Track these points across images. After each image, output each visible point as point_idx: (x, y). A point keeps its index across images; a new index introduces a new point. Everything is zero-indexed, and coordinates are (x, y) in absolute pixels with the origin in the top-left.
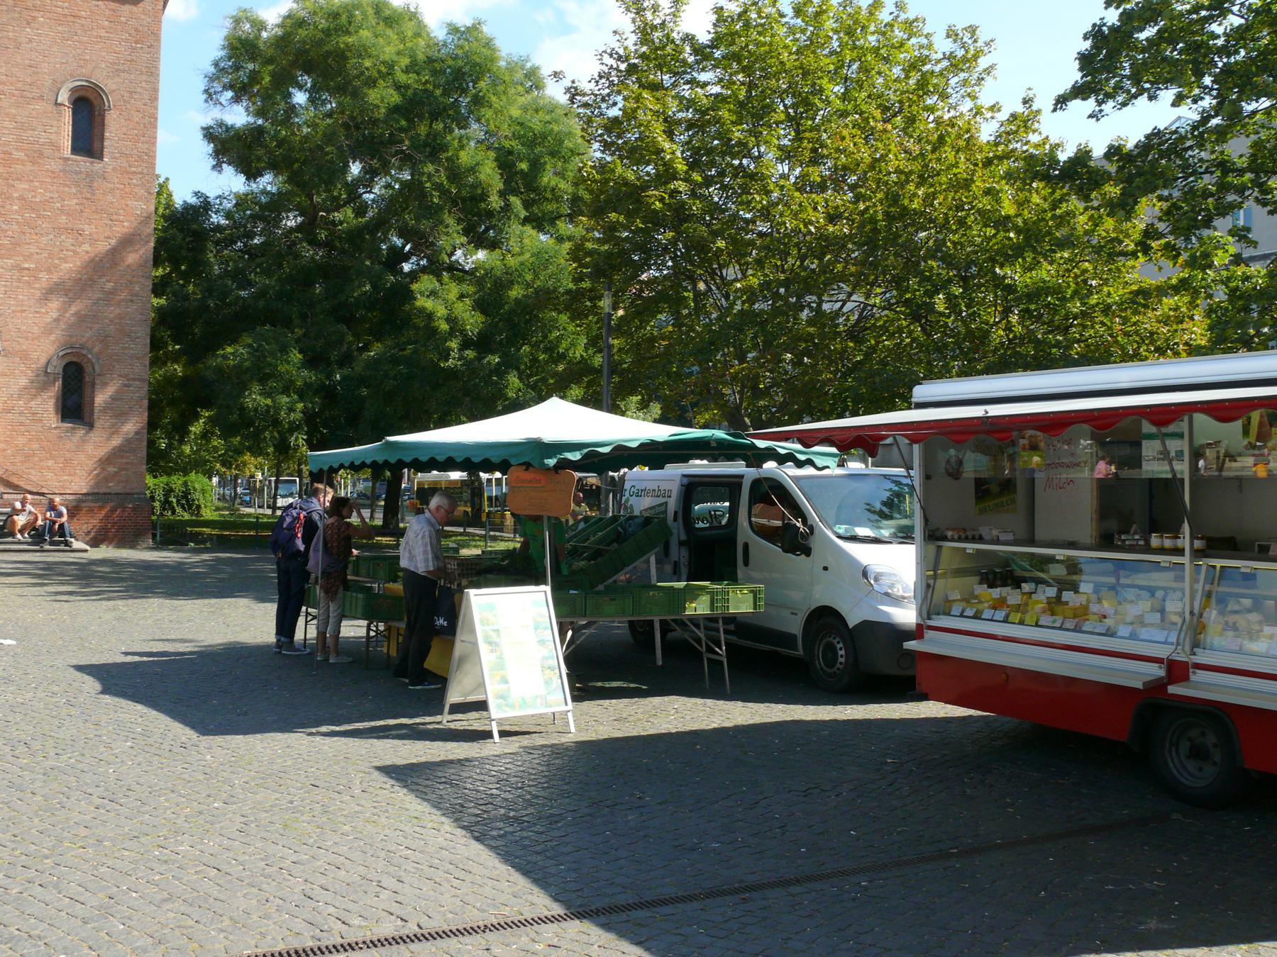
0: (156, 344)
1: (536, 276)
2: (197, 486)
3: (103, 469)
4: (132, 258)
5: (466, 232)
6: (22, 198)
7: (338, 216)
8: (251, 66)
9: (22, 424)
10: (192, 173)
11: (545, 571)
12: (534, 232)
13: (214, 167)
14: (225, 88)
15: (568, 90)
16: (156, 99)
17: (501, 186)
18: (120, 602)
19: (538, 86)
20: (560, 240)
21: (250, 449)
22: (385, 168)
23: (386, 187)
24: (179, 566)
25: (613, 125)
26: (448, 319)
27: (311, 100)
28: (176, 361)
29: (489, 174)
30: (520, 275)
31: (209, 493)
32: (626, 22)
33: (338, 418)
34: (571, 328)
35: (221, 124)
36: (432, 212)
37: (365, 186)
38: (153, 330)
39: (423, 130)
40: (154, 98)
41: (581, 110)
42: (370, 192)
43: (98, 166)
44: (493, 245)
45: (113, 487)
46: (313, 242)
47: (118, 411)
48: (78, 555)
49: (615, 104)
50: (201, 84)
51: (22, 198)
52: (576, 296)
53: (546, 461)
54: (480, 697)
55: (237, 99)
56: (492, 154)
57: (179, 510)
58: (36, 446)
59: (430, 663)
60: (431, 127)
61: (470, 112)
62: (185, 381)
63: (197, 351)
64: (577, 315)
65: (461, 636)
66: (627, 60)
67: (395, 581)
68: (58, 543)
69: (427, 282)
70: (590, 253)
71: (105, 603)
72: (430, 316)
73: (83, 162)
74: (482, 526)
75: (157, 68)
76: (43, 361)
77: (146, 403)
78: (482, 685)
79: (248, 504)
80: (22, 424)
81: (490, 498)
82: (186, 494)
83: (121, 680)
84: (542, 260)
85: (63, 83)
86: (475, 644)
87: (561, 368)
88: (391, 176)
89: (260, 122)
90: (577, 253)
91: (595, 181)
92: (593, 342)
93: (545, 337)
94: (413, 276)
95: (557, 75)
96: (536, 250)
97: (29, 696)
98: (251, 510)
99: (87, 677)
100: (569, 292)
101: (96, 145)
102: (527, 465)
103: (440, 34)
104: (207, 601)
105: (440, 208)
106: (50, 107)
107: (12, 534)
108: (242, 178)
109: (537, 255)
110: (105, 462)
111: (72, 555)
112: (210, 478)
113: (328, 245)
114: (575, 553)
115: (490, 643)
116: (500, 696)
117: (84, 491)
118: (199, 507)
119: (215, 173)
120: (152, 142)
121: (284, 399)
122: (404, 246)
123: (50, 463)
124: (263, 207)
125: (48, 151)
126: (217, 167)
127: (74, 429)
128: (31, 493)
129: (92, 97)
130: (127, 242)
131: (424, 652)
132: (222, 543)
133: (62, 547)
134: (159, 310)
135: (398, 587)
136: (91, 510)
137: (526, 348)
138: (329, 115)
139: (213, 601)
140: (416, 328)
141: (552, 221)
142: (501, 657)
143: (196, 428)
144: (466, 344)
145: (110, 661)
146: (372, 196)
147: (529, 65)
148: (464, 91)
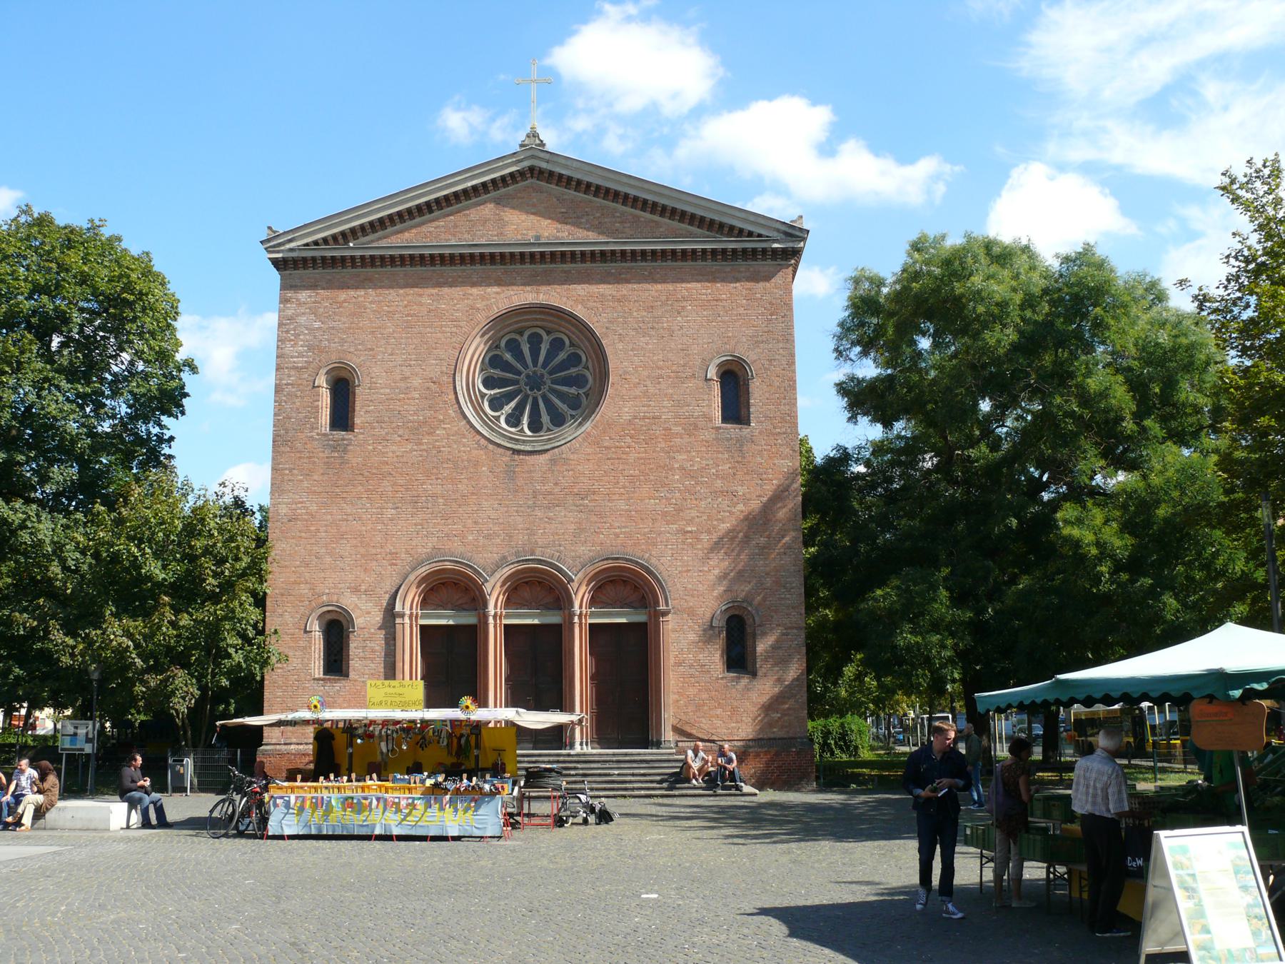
0: (810, 592)
1: (1183, 493)
2: (853, 727)
3: (766, 715)
4: (782, 514)
5: (1104, 455)
6: (682, 468)
7: (973, 453)
8: (875, 321)
9: (692, 676)
10: (829, 427)
11: (1239, 807)
12: (1174, 448)
13: (849, 419)
14: (853, 344)
15: (1195, 298)
16: (793, 363)
17: (1134, 408)
18: (793, 845)
19: (1161, 297)
20: (1205, 453)
21: (901, 687)
22: (1014, 402)
23: (1017, 419)
24: (845, 807)
25: (1250, 329)
26: (1098, 544)
27: (936, 345)
28: (827, 606)
29: (1121, 396)
30: (1166, 493)
31: (865, 733)
32: (1244, 222)
33: (999, 653)
34: (1227, 542)
35: (852, 378)
36: (1068, 440)
37: (997, 421)
38: (806, 578)
39: (1047, 359)
40: (791, 363)
41: (1212, 317)
42: (1003, 426)
43: (746, 431)
44: (1131, 466)
45: (777, 732)
46: (953, 482)
47: (780, 657)
48: (748, 798)
49: (1247, 306)
50: (832, 344)
51: (682, 468)
52: (1227, 510)
53: (1231, 693)
54: (1179, 947)
55: (865, 353)
56: (1120, 378)
57: (837, 751)
58: (705, 696)
59: (1124, 906)
60: (1056, 355)
61: (1093, 336)
62: (837, 626)
63: (849, 595)
64: (1233, 528)
65: (1153, 881)
66: (1254, 260)
67: (1072, 822)
68: (729, 788)
69: (1068, 512)
70: (1241, 462)
71: (779, 846)
72: (1077, 544)
73: (733, 429)
74: (1145, 756)
75: (792, 335)
76: (708, 615)
77: (804, 650)
78: (1180, 934)
79: (902, 743)
80: (692, 676)
81: (1153, 727)
82: (843, 736)
83: (805, 922)
84: (1188, 475)
85: (711, 360)
86: (1170, 889)
87: (1220, 585)
88: (1022, 408)
89: (889, 371)
90: (1226, 462)
91: (1238, 388)
92: (1253, 555)
93: (1199, 554)
94: (1054, 505)
95: (1182, 283)
96: (1185, 464)
97: (723, 937)
98: (906, 749)
99: (773, 921)
100: (1221, 505)
101: (743, 412)
102: (1211, 698)
103: (1055, 265)
104: (876, 843)
105: (1075, 435)
106: (701, 384)
107: (689, 781)
108: (879, 427)
109: (1182, 471)
110: (768, 708)
111: (743, 798)
112: (866, 719)
113: (966, 483)
114: (1265, 786)
115: (1186, 889)
116: (1202, 947)
117: (751, 737)
118: (856, 748)
119: (851, 425)
120: (793, 403)
121: (935, 638)
122: (1041, 476)
123: (719, 711)
124: (899, 452)
125: (701, 424)
126: (853, 419)
127: (739, 678)
128: (702, 740)
129: (734, 368)
130: (778, 497)
131: (1115, 897)
132: (883, 784)
133: (733, 791)
134: (814, 558)
135: (1076, 827)
136: (757, 755)
137: (1180, 568)
138: (955, 356)
139: (882, 843)
140: (1062, 557)
141: (1196, 435)
142: (1199, 904)
143: (849, 671)
144: (1118, 567)
145: (792, 904)
146: (1005, 430)
147: (1148, 279)
148: (1084, 316)
